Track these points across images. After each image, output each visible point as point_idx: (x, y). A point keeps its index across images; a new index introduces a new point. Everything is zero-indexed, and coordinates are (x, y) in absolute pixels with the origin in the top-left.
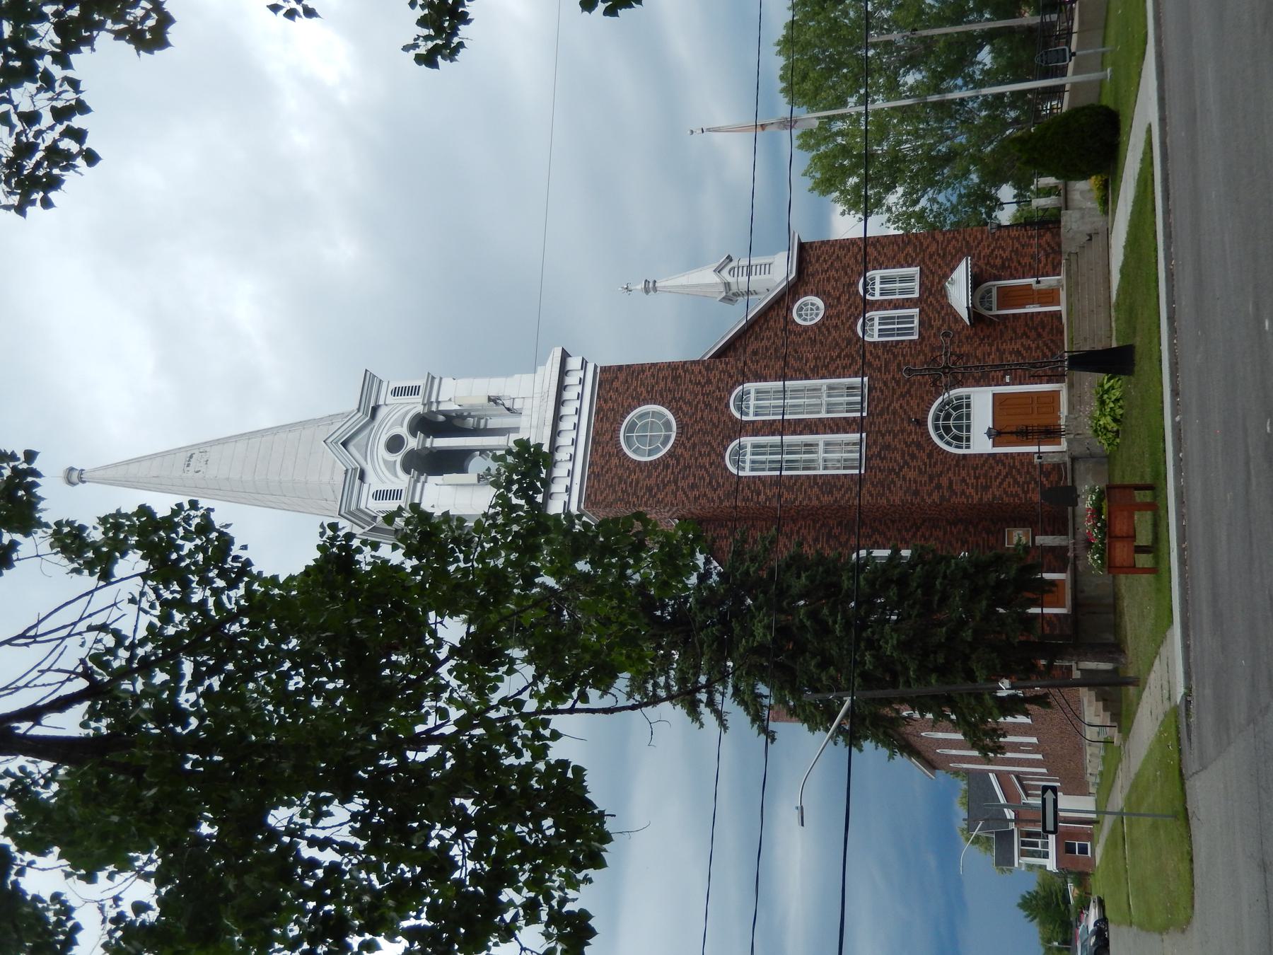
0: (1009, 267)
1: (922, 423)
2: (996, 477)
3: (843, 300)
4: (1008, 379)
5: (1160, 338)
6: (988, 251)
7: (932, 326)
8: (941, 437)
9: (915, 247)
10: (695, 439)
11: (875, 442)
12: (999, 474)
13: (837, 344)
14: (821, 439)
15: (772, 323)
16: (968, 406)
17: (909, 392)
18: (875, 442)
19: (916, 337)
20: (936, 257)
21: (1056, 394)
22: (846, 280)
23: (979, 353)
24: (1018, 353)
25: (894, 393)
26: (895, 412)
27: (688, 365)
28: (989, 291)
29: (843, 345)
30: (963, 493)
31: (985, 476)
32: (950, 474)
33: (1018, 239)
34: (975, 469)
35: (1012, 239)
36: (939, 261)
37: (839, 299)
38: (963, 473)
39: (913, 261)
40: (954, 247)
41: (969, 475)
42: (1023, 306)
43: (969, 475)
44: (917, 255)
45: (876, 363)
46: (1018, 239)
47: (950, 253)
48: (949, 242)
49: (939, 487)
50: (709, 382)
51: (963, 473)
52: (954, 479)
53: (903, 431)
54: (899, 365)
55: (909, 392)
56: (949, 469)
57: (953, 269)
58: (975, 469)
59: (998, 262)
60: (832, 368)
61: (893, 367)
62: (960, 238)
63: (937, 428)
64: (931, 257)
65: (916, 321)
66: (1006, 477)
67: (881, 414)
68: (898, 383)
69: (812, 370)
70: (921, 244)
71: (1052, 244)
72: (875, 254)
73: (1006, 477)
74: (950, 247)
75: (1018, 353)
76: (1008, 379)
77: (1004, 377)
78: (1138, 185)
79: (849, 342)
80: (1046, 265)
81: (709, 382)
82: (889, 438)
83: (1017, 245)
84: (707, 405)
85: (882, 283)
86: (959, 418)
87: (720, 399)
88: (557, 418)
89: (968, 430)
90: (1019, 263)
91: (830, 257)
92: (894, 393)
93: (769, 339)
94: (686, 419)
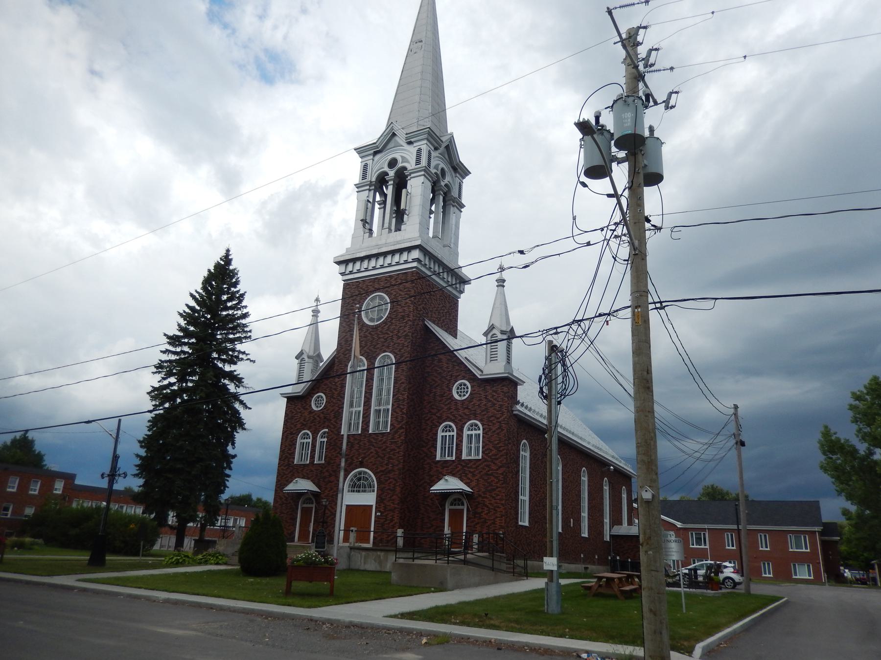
1: (362, 465)
3: (466, 411)
4: (378, 514)
5: (219, 597)
6: (487, 503)
7: (443, 468)
8: (355, 476)
9: (496, 455)
10: (369, 337)
11: (355, 439)
13: (439, 411)
14: (373, 408)
15: (457, 368)
17: (379, 456)
18: (355, 439)
19: (36, 493)
20: (487, 469)
21: (368, 541)
22: (479, 411)
23: (394, 497)
24: (392, 521)
25: (380, 448)
26: (369, 449)
27: (362, 334)
29: (438, 415)
30: (326, 489)
37: (467, 408)
39: (487, 454)
42: (450, 525)
44: (490, 457)
45: (397, 436)
46: (494, 523)
48: (495, 477)
49: (330, 475)
50: (399, 337)
53: (359, 454)
54: (394, 450)
55: (379, 456)
59: (480, 510)
60: (397, 410)
61: (393, 446)
63: (360, 473)
64: (487, 466)
65: (449, 458)
67: (369, 441)
68: (384, 450)
69: (397, 398)
70: (497, 459)
72: (494, 429)
74: (493, 478)
75: (392, 521)
76: (378, 514)
77: (380, 511)
78: (446, 606)
79: (440, 418)
81: (399, 337)
82: (356, 447)
83: (489, 522)
84: (386, 339)
85: (476, 435)
87: (388, 347)
88: (385, 254)
90: (478, 523)
91: (495, 399)
92: (380, 448)
93: (447, 368)
94: (380, 329)
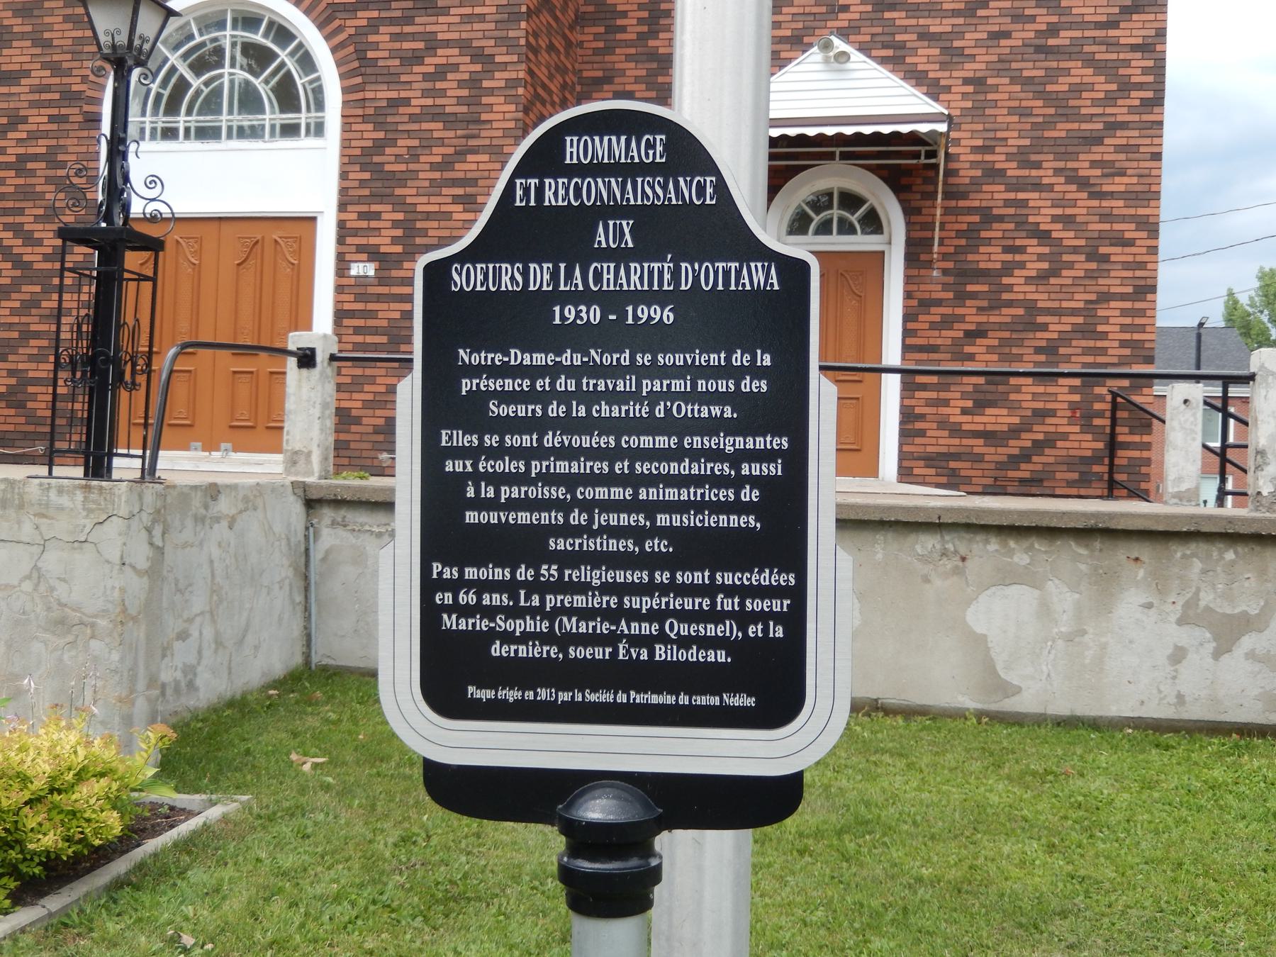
0: (961, 297)
2: (17, 230)
4: (363, 269)
6: (1043, 212)
12: (29, 240)
16: (290, 130)
28: (873, 223)
31: (26, 193)
32: (40, 75)
33: (1087, 331)
34: (51, 159)
35: (1089, 310)
36: (1023, 34)
38: (38, 119)
40: (1077, 90)
41: (33, 136)
43: (33, 136)
46: (1087, 331)
47: (1052, 76)
51: (38, 119)
52: (23, 88)
56: (55, 69)
57: (895, 58)
58: (51, 159)
62: (1120, 113)
66: (18, 262)
71: (1049, 456)
73: (18, 262)
74: (1080, 73)
76: (363, 269)
77: (372, 254)
80: (956, 431)
83: (1057, 326)
86: (249, 100)
89: (206, 133)
